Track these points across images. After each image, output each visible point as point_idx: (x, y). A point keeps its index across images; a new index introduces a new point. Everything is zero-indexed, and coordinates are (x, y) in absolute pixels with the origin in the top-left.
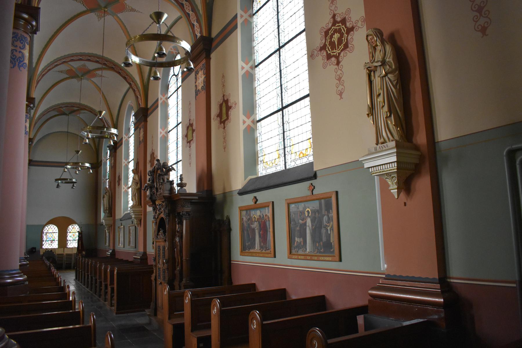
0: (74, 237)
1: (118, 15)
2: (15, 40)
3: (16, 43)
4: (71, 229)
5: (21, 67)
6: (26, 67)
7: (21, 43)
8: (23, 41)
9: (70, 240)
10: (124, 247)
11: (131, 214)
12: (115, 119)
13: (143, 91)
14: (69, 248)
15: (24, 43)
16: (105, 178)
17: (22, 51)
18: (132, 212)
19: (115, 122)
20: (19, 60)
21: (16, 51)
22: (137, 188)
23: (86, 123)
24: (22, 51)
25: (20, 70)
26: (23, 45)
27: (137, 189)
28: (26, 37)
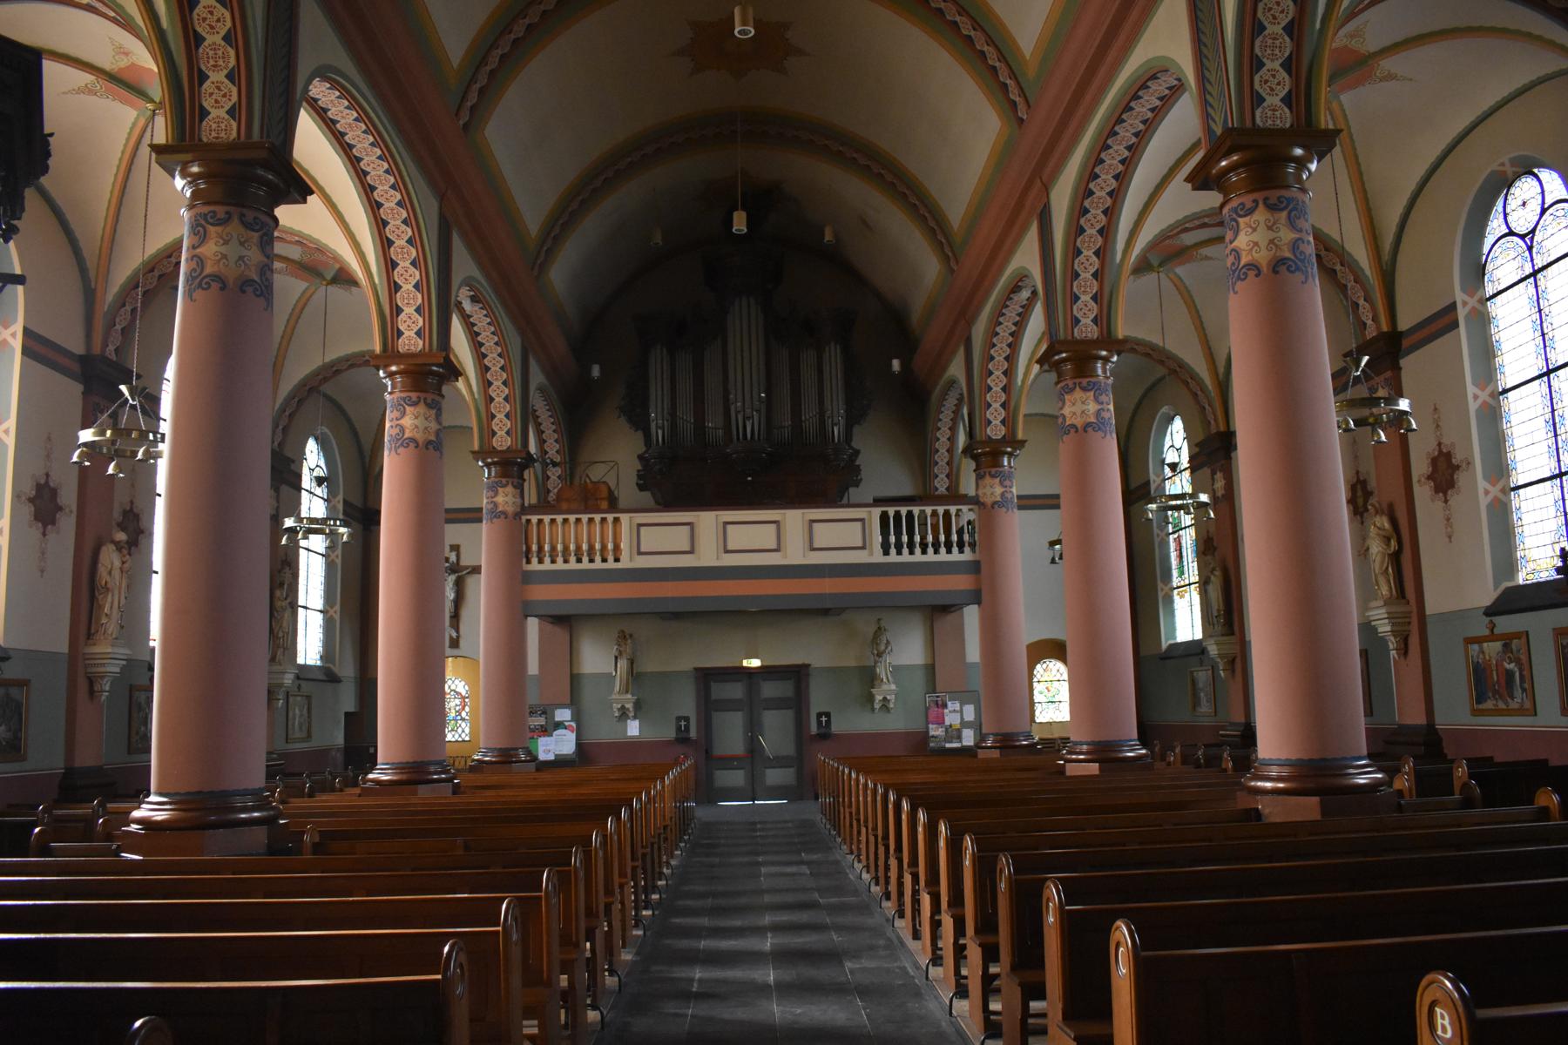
0: (1051, 694)
4: (1042, 671)
5: (195, 290)
9: (1039, 703)
10: (1216, 715)
12: (1221, 370)
14: (1041, 723)
16: (1162, 530)
18: (1386, 616)
19: (1221, 377)
22: (1390, 552)
27: (1389, 555)
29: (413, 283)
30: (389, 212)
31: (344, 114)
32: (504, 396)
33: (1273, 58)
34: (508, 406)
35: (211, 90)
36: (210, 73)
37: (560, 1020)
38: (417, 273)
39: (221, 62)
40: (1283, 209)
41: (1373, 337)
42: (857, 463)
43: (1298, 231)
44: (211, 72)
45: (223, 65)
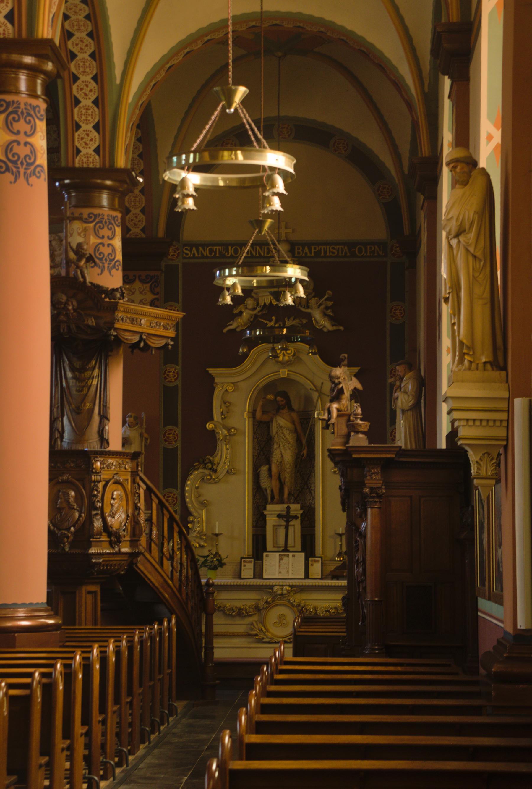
6: (42, 174)
7: (108, 228)
8: (112, 224)
13: (256, 660)
15: (113, 228)
20: (108, 260)
21: (19, 143)
28: (38, 106)
30: (82, 28)
32: (79, 82)
33: (87, 121)
36: (91, 105)
37: (285, 195)
39: (84, 111)
41: (47, 111)
45: (82, 109)
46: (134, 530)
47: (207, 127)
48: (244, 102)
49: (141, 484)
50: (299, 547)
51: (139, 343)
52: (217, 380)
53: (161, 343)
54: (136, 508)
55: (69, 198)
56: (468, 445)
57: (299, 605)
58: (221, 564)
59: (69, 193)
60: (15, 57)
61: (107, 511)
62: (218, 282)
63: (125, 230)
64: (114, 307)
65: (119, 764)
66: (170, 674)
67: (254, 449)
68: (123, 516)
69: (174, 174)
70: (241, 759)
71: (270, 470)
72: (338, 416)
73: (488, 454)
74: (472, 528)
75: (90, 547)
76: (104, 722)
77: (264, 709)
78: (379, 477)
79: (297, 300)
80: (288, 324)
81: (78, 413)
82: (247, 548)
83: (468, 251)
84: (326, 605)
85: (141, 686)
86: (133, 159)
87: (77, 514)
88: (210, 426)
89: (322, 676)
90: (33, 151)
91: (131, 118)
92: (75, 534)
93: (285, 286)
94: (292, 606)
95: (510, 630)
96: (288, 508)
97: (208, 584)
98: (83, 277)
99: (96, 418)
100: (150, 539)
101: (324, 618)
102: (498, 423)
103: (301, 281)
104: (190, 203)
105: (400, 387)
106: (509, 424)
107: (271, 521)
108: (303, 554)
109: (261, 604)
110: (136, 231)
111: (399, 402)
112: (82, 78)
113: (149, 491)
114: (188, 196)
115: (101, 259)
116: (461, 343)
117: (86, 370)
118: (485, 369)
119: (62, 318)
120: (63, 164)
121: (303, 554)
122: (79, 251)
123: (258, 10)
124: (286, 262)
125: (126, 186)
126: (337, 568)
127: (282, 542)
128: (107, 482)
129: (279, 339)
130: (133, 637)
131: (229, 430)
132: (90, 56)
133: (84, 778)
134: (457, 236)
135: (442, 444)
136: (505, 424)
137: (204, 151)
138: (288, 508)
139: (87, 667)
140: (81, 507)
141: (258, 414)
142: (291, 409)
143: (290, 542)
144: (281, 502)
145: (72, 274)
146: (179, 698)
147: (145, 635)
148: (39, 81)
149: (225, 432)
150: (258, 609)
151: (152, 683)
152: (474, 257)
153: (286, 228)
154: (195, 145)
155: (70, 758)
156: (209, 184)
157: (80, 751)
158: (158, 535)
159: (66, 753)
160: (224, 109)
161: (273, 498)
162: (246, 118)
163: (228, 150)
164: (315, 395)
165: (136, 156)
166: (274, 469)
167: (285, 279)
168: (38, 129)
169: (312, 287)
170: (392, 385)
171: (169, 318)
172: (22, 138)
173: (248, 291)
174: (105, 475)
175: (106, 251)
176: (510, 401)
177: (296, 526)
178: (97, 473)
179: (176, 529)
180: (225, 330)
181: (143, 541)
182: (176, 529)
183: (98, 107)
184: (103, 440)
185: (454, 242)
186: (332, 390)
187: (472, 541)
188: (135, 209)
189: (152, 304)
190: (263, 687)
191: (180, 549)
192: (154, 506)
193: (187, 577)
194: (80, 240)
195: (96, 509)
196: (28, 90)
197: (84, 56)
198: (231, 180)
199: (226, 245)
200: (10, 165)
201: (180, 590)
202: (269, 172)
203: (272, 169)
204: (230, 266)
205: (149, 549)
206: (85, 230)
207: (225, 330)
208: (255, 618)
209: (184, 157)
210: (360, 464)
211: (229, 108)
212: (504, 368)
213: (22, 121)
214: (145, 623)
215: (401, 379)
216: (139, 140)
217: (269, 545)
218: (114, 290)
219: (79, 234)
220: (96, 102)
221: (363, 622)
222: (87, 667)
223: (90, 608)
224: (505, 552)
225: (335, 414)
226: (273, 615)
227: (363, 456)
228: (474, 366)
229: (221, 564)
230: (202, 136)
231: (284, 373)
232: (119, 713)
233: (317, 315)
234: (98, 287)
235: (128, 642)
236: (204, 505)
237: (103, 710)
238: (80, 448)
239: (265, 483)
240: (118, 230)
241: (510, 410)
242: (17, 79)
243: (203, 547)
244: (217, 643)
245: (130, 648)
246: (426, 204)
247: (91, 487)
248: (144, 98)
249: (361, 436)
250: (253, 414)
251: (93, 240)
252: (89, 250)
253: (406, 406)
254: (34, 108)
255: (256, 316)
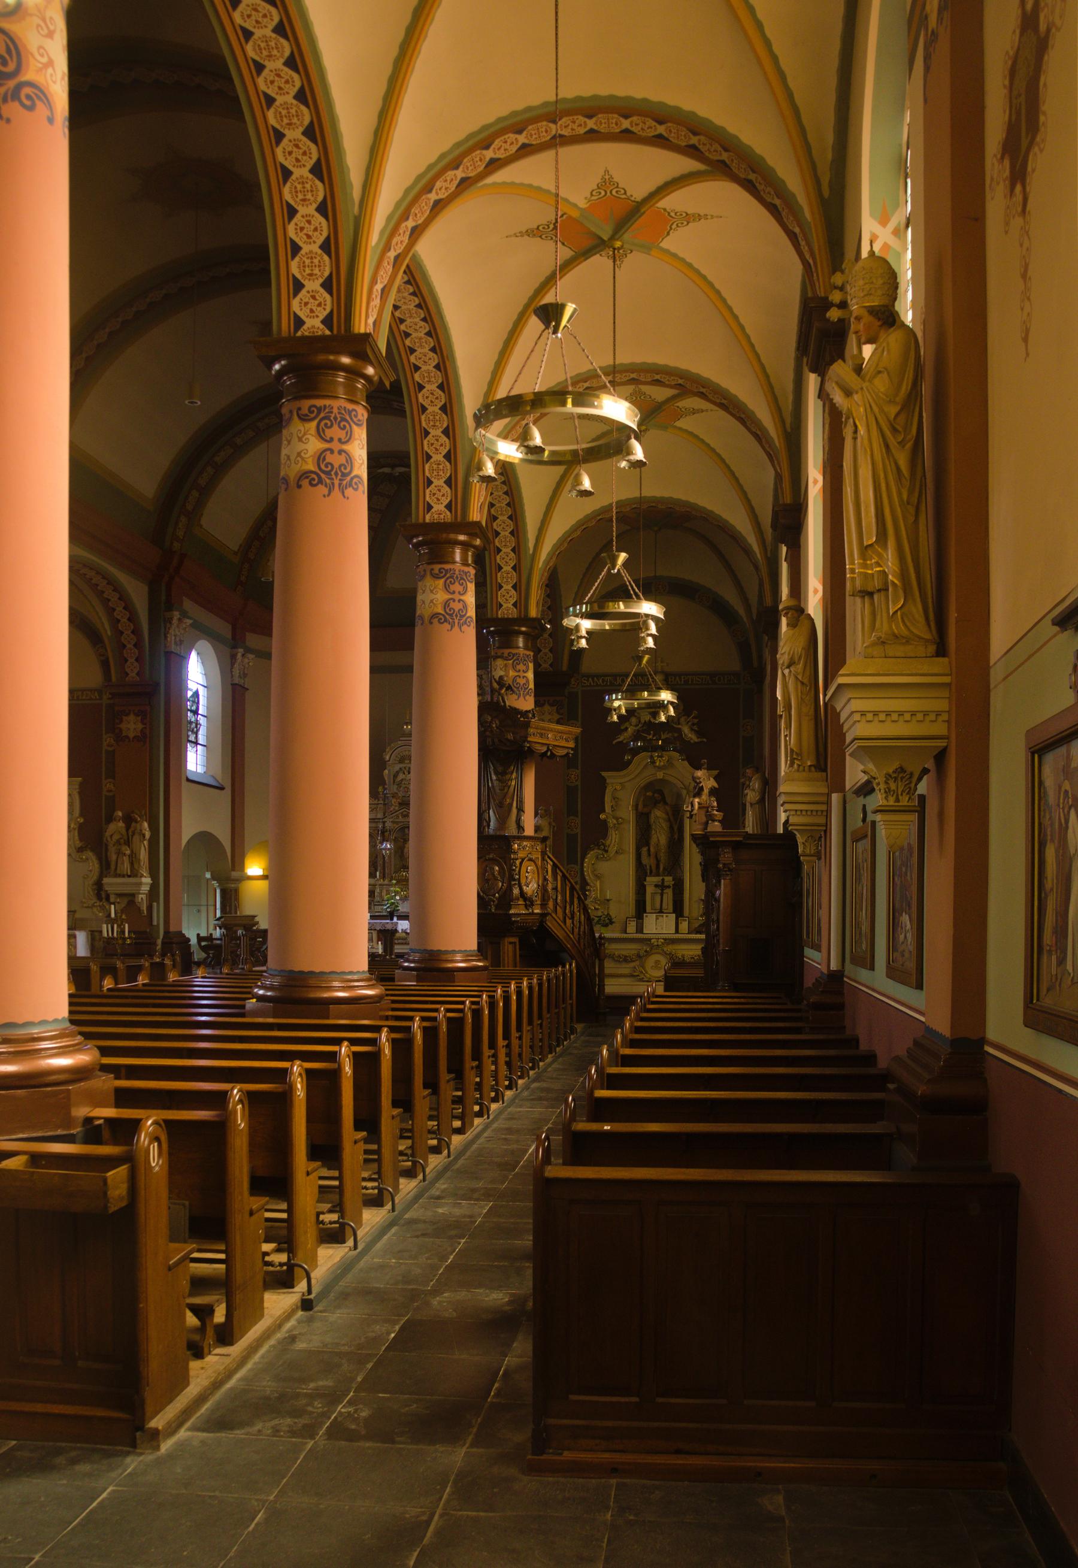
1: (661, 245)
2: (326, 425)
3: (329, 433)
11: (320, 1405)
17: (345, 447)
21: (332, 451)
23: (588, 569)
24: (345, 447)
25: (344, 497)
26: (347, 433)
29: (285, 141)
31: (403, 300)
34: (287, 196)
35: (307, 300)
38: (421, 400)
40: (312, 419)
41: (476, 575)
42: (282, 474)
43: (326, 441)
44: (307, 281)
45: (319, 274)
46: (543, 896)
47: (596, 584)
48: (625, 564)
49: (549, 861)
50: (671, 909)
51: (547, 751)
52: (608, 781)
53: (563, 752)
54: (545, 879)
55: (494, 641)
56: (796, 830)
57: (185, 629)
58: (611, 923)
59: (493, 638)
60: (452, 536)
61: (523, 881)
62: (607, 704)
63: (537, 666)
64: (527, 725)
65: (532, 1068)
66: (571, 1004)
67: (637, 834)
68: (535, 886)
69: (571, 620)
70: (617, 1066)
71: (649, 850)
72: (699, 808)
73: (812, 837)
74: (801, 895)
75: (510, 909)
76: (520, 1038)
77: (638, 1030)
78: (730, 855)
79: (669, 717)
80: (663, 737)
81: (501, 807)
82: (631, 910)
83: (797, 678)
84: (691, 953)
85: (548, 1012)
86: (543, 611)
87: (500, 884)
88: (602, 816)
89: (683, 1006)
90: (465, 606)
91: (541, 579)
92: (499, 899)
93: (659, 707)
94: (665, 954)
95: (826, 972)
96: (663, 880)
97: (600, 938)
98: (504, 701)
99: (514, 810)
100: (556, 903)
101: (689, 963)
102: (819, 813)
103: (672, 703)
104: (583, 643)
105: (749, 786)
106: (828, 814)
107: (650, 890)
108: (674, 915)
109: (642, 953)
110: (545, 666)
111: (748, 797)
112: (504, 550)
113: (555, 866)
114: (582, 637)
115: (518, 688)
116: (792, 751)
117: (506, 774)
118: (810, 771)
119: (488, 733)
120: (489, 616)
121: (674, 915)
122: (501, 682)
123: (637, 495)
124: (661, 689)
125: (537, 631)
126: (700, 926)
127: (658, 906)
128: (523, 860)
129: (656, 748)
130: (542, 976)
131: (617, 819)
132: (510, 533)
133: (506, 1077)
134: (788, 667)
135: (780, 830)
136: (825, 813)
137: (595, 602)
138: (663, 880)
139: (507, 998)
140: (503, 878)
141: (640, 807)
142: (665, 803)
143: (664, 906)
144: (658, 875)
145: (495, 700)
146: (578, 1021)
147: (552, 975)
148: (470, 553)
149: (615, 821)
150: (639, 956)
151: (557, 1011)
152: (802, 683)
153: (662, 662)
154: (587, 598)
155: (495, 1063)
156: (598, 628)
157: (502, 1058)
158: (561, 900)
159: (491, 1059)
160: (609, 570)
161: (651, 872)
162: (627, 577)
163: (612, 601)
164: (684, 792)
165: (545, 608)
166: (652, 850)
167: (659, 701)
168: (469, 589)
169: (682, 707)
170: (744, 784)
171: (569, 733)
172: (456, 597)
173: (631, 712)
174: (521, 855)
175: (522, 681)
176: (829, 796)
177: (669, 894)
178: (515, 853)
179: (576, 895)
180: (614, 742)
181: (551, 904)
182: (576, 895)
183: (516, 571)
184: (520, 827)
185: (786, 671)
186: (695, 788)
187: (801, 903)
188: (438, 479)
189: (558, 722)
190: (637, 1014)
191: (579, 911)
192: (559, 878)
193: (584, 932)
194: (502, 673)
195: (515, 880)
196: (461, 560)
197: (505, 534)
198: (615, 624)
199: (615, 676)
200: (447, 617)
201: (579, 942)
202: (644, 618)
203: (647, 616)
204: (616, 692)
205: (556, 911)
206: (506, 665)
207: (614, 742)
208: (637, 963)
209: (578, 607)
210: (716, 845)
211: (614, 569)
212: (825, 770)
213: (457, 584)
214: (551, 966)
215: (750, 779)
216: (548, 596)
217: (648, 908)
218: (526, 711)
219: (501, 669)
220: (514, 568)
221: (717, 965)
222: (507, 998)
223: (511, 954)
224: (823, 913)
225: (696, 806)
226: (650, 961)
227: (718, 839)
228: (801, 768)
229: (611, 923)
230: (592, 592)
231: (660, 775)
232: (532, 1031)
233: (686, 730)
234: (515, 709)
235: (538, 980)
236: (598, 877)
237: (519, 1028)
238: (502, 833)
239: (645, 860)
240: (531, 665)
241: (828, 803)
242: (453, 553)
243: (598, 909)
244: (608, 981)
245: (540, 985)
246: (769, 644)
247: (510, 863)
248: (551, 564)
249: (716, 823)
250: (636, 807)
251: (512, 673)
252: (508, 681)
253: (754, 801)
254: (466, 573)
255: (638, 731)
